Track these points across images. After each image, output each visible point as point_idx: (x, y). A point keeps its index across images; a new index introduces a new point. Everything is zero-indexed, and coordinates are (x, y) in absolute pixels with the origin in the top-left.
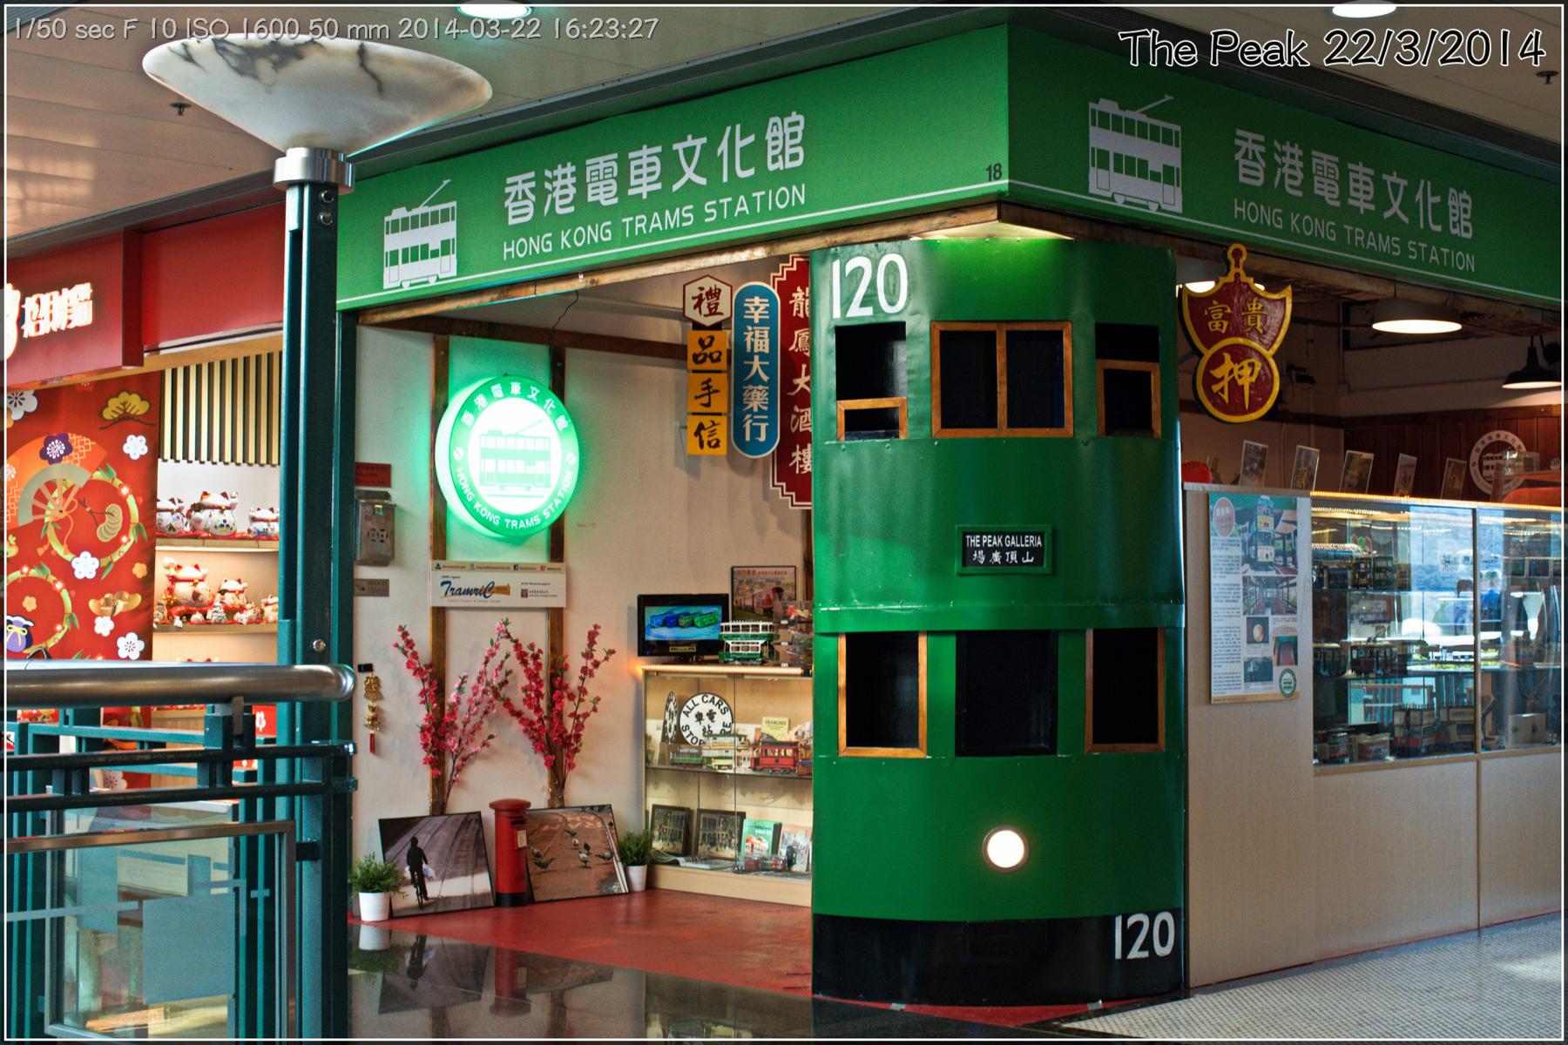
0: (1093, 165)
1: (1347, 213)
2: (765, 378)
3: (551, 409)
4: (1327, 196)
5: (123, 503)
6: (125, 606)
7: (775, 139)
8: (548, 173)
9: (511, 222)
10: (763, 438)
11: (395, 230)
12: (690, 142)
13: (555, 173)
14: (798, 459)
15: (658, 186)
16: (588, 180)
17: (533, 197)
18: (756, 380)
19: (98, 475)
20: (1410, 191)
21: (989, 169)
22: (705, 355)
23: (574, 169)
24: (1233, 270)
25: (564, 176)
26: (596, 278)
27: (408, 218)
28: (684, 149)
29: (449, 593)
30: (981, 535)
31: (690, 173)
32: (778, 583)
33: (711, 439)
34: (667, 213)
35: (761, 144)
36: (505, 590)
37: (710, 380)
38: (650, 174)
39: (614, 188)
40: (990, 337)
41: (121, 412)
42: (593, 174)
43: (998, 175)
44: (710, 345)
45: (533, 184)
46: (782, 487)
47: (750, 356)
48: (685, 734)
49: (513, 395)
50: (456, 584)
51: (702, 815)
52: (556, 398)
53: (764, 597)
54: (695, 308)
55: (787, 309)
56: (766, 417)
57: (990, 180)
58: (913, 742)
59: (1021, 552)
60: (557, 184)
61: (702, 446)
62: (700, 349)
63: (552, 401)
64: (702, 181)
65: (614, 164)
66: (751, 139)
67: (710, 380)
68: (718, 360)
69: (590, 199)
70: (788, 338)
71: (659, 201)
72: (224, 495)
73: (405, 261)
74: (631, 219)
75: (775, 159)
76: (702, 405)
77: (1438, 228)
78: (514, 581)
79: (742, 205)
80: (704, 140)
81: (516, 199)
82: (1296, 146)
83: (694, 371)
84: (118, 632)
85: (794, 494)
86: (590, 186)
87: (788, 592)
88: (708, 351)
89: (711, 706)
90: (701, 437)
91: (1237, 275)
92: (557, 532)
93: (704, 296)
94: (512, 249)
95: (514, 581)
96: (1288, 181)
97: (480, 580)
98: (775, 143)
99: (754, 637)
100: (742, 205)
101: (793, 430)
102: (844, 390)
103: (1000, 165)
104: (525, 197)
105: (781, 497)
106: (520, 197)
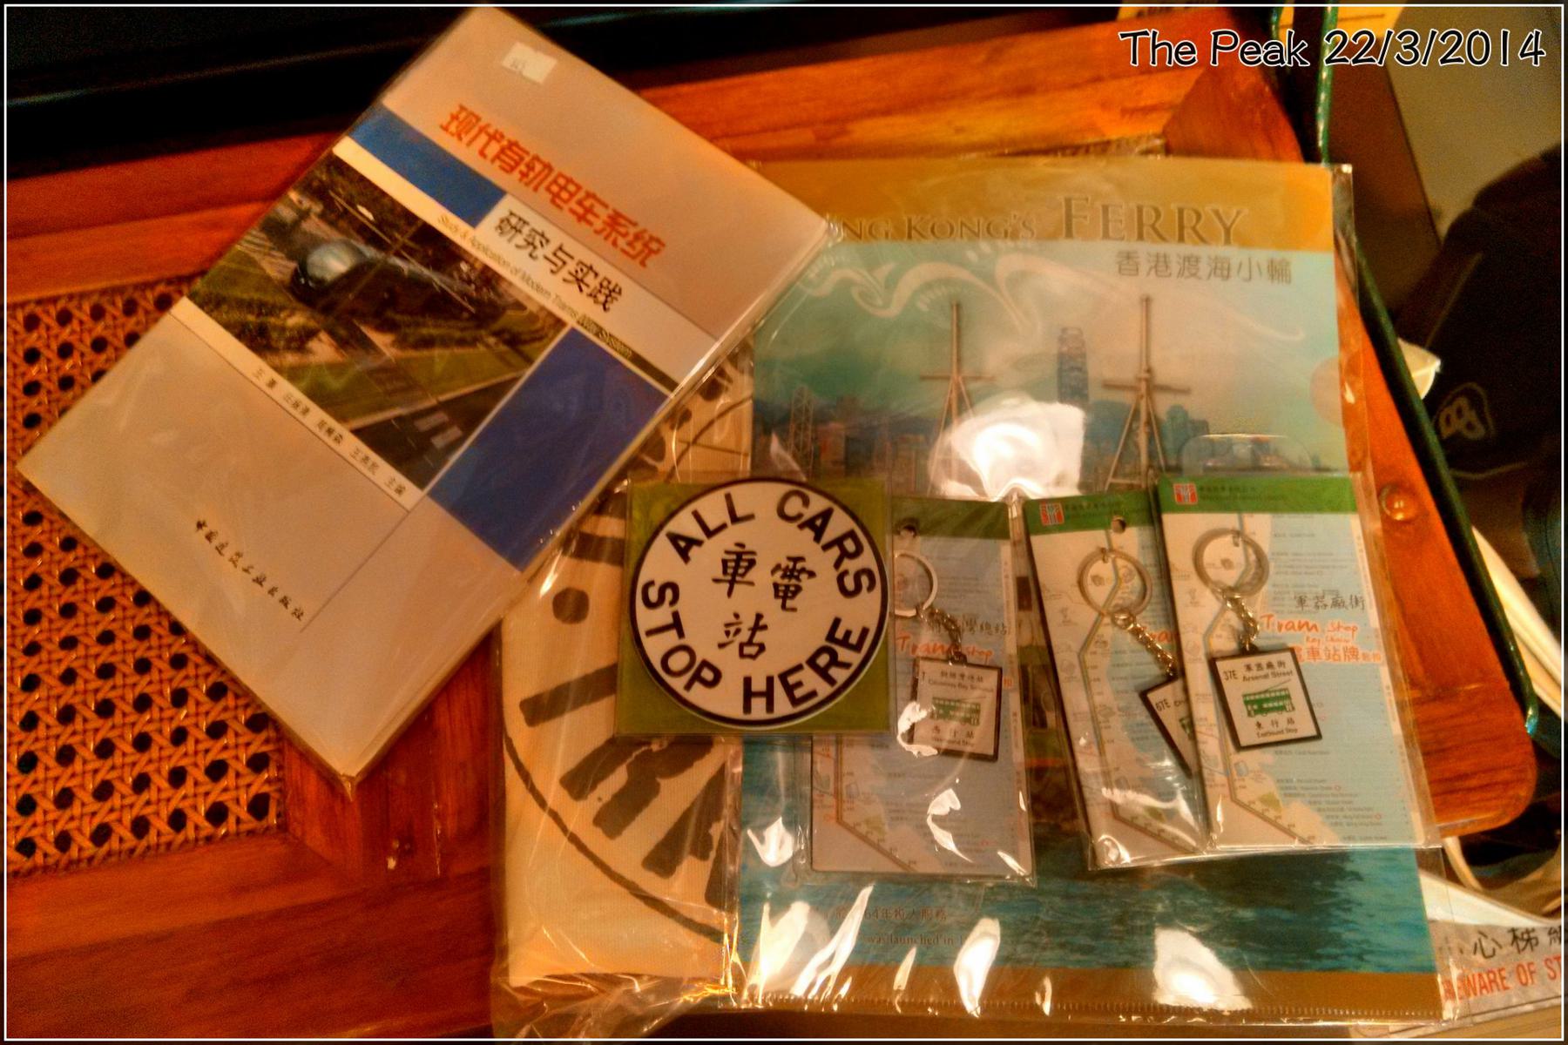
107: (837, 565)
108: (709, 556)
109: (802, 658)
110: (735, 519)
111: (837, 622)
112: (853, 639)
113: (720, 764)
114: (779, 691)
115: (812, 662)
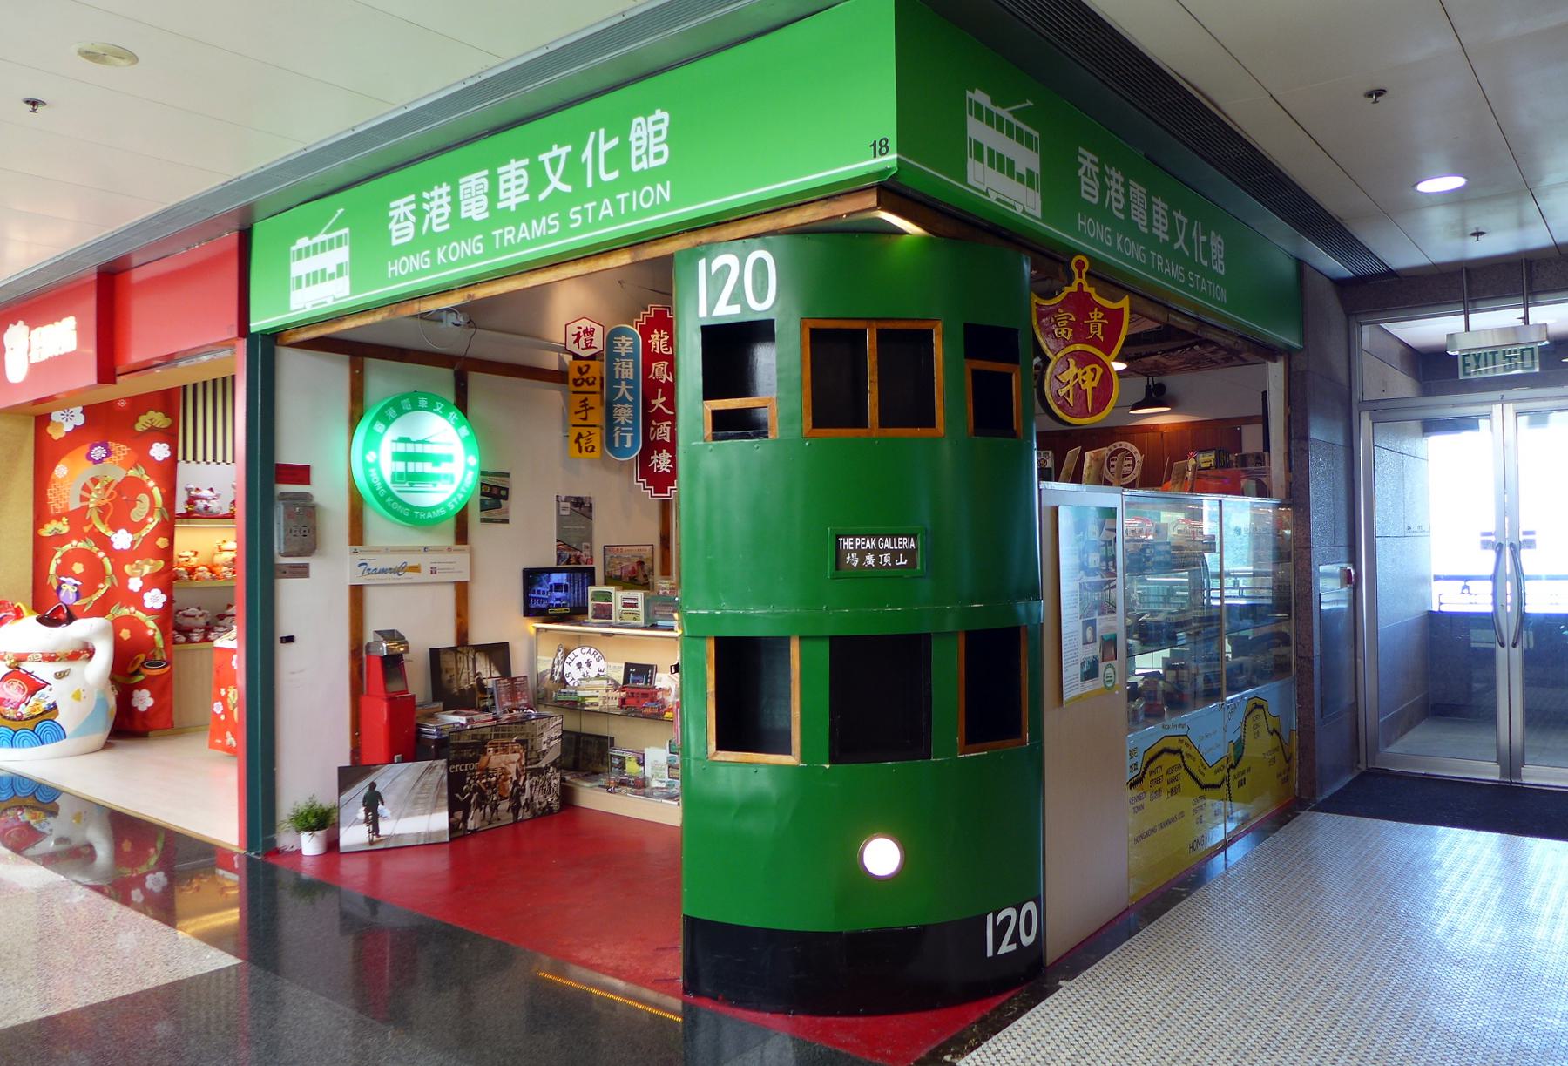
0: (971, 156)
1: (1149, 240)
2: (630, 399)
3: (455, 420)
4: (1140, 222)
5: (149, 492)
6: (151, 569)
7: (639, 139)
8: (426, 195)
9: (395, 242)
10: (628, 445)
11: (300, 258)
12: (555, 151)
13: (433, 193)
15: (526, 197)
16: (461, 198)
17: (413, 218)
18: (623, 400)
19: (132, 472)
20: (1190, 227)
21: (874, 145)
22: (583, 379)
23: (448, 188)
24: (1077, 281)
25: (440, 196)
26: (472, 293)
27: (309, 247)
28: (550, 160)
29: (366, 573)
30: (855, 536)
31: (555, 182)
32: (641, 557)
34: (534, 222)
35: (625, 146)
36: (416, 569)
37: (586, 399)
38: (518, 186)
39: (485, 203)
40: (861, 334)
41: (149, 426)
42: (466, 191)
43: (884, 150)
44: (587, 371)
45: (413, 206)
46: (643, 482)
47: (619, 382)
48: (568, 680)
49: (421, 409)
50: (372, 566)
52: (460, 413)
53: (630, 569)
54: (574, 343)
55: (647, 346)
56: (631, 429)
57: (875, 156)
58: (788, 751)
59: (895, 554)
60: (434, 204)
61: (580, 451)
62: (579, 375)
63: (455, 414)
64: (567, 188)
65: (485, 181)
66: (615, 142)
67: (586, 399)
68: (593, 383)
69: (463, 215)
70: (647, 369)
71: (528, 211)
72: (211, 490)
73: (308, 284)
74: (501, 231)
75: (639, 159)
76: (581, 419)
77: (1205, 263)
78: (425, 561)
79: (606, 208)
80: (569, 148)
81: (398, 222)
82: (1119, 172)
83: (574, 393)
84: (144, 590)
85: (652, 488)
86: (463, 204)
87: (648, 565)
88: (585, 377)
91: (1080, 285)
92: (462, 519)
93: (582, 334)
94: (395, 268)
95: (425, 561)
96: (1115, 204)
97: (395, 561)
98: (639, 143)
100: (606, 208)
101: (652, 439)
102: (711, 390)
103: (886, 140)
104: (406, 219)
105: (635, 483)
106: (402, 219)
108: (574, 664)
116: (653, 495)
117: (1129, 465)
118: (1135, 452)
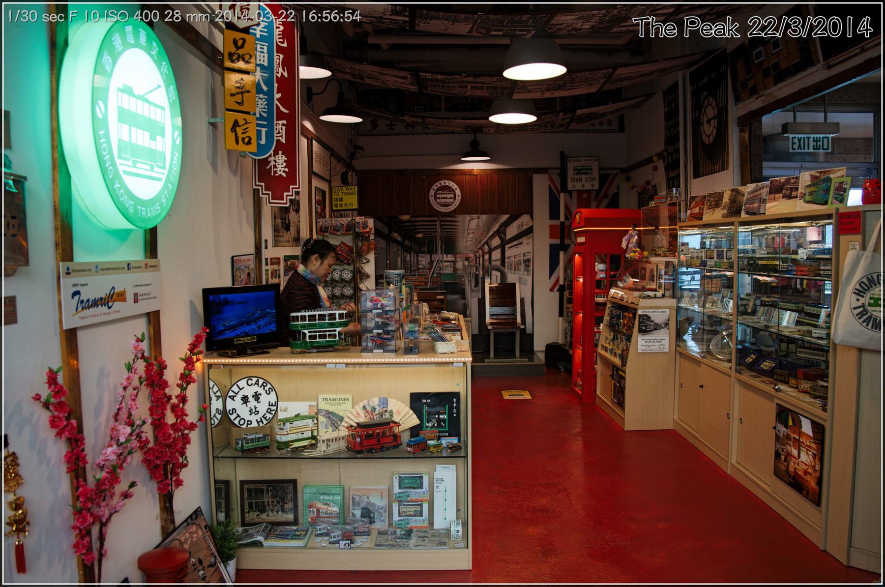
2: (265, 88)
14: (273, 163)
33: (244, 136)
48: (232, 417)
51: (246, 486)
61: (237, 143)
89: (255, 388)
90: (236, 135)
99: (332, 325)
107: (264, 389)
108: (238, 398)
109: (265, 412)
110: (241, 389)
111: (269, 402)
112: (274, 404)
113: (557, 277)
114: (263, 419)
115: (267, 412)
116: (271, 201)
117: (451, 198)
118: (456, 189)
